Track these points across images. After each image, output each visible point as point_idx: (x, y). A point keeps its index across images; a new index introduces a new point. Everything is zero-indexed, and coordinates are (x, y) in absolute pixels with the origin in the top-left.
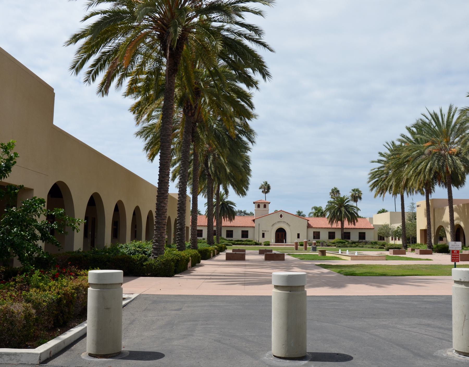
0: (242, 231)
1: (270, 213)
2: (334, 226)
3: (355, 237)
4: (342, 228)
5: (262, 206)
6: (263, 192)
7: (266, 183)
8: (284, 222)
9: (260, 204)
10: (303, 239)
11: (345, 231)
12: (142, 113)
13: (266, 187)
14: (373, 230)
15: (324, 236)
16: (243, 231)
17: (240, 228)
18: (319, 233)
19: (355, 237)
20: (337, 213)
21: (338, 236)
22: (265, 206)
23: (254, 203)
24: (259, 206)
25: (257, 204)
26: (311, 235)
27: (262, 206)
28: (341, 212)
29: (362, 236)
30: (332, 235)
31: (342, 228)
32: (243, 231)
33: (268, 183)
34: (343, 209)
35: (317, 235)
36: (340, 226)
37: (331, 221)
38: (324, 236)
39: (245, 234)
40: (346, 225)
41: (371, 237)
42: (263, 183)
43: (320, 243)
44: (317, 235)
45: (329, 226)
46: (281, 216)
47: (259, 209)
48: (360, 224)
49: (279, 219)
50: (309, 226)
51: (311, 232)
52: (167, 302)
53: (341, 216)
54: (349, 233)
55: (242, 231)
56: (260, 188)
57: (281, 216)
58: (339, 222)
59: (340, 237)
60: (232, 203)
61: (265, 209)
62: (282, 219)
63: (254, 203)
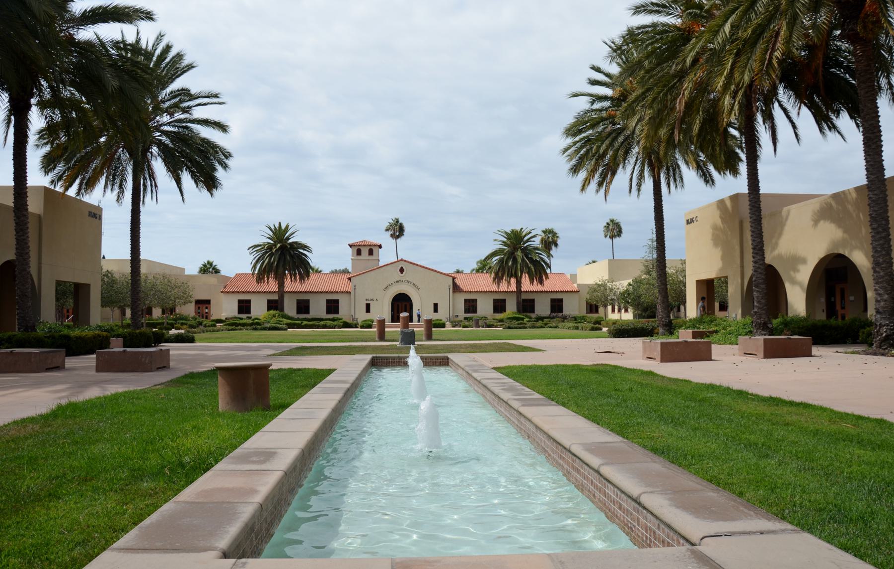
1: (381, 264)
2: (504, 287)
4: (519, 291)
5: (365, 251)
7: (397, 222)
8: (408, 282)
9: (361, 248)
11: (524, 297)
14: (576, 295)
15: (485, 308)
16: (553, 301)
17: (323, 295)
19: (543, 308)
21: (511, 308)
22: (371, 252)
24: (359, 252)
26: (461, 306)
27: (365, 251)
28: (515, 260)
30: (499, 306)
31: (519, 291)
32: (553, 301)
34: (519, 254)
35: (471, 306)
36: (513, 287)
37: (498, 279)
38: (485, 308)
39: (333, 306)
40: (527, 285)
44: (471, 306)
45: (494, 288)
46: (402, 270)
47: (359, 257)
49: (398, 276)
50: (456, 288)
51: (460, 300)
56: (387, 230)
57: (402, 270)
58: (513, 280)
59: (515, 309)
60: (305, 247)
61: (371, 257)
63: (351, 246)
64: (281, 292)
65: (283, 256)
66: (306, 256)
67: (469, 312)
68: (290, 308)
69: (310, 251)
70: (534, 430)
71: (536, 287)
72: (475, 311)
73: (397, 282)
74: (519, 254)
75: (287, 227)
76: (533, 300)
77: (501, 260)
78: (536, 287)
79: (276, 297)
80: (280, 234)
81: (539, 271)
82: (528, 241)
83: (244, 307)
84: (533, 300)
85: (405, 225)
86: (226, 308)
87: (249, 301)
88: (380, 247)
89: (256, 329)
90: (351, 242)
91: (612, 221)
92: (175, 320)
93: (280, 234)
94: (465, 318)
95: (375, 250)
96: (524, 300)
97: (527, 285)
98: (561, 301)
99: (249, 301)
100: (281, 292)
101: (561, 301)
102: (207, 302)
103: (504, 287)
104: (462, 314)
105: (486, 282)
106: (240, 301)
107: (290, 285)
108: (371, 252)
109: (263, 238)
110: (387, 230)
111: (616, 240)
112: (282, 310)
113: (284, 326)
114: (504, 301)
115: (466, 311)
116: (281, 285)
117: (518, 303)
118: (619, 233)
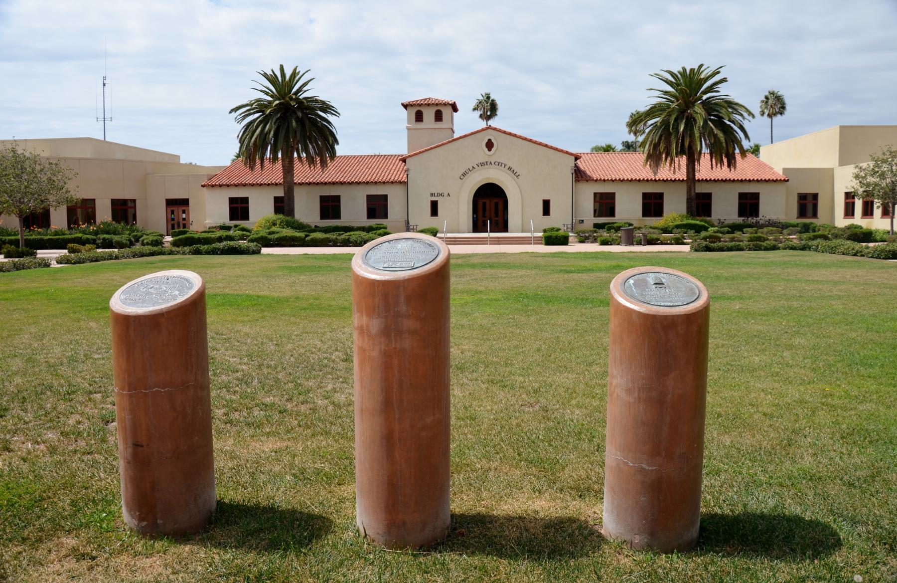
0: (369, 197)
1: (456, 136)
2: (665, 172)
3: (725, 209)
4: (691, 179)
5: (429, 115)
6: (481, 116)
7: (488, 98)
9: (423, 109)
10: (559, 219)
11: (700, 189)
12: (605, 234)
13: (488, 106)
14: (781, 187)
15: (628, 208)
16: (742, 196)
17: (361, 187)
18: (612, 196)
19: (725, 209)
20: (676, 128)
21: (675, 208)
22: (439, 117)
23: (405, 106)
24: (419, 117)
25: (414, 110)
26: (588, 205)
27: (429, 115)
28: (690, 122)
29: (749, 204)
30: (653, 205)
31: (691, 179)
32: (742, 196)
33: (492, 97)
34: (699, 110)
35: (605, 204)
36: (682, 174)
37: (654, 158)
38: (628, 208)
40: (706, 169)
41: (776, 207)
42: (481, 98)
43: (618, 229)
44: (605, 204)
45: (646, 173)
46: (490, 145)
47: (419, 125)
48: (745, 169)
49: (483, 154)
50: (579, 175)
51: (587, 193)
52: (473, 266)
53: (692, 136)
54: (709, 196)
55: (369, 197)
56: (475, 109)
57: (490, 145)
58: (684, 160)
59: (683, 208)
60: (326, 107)
61: (439, 125)
62: (495, 155)
63: (405, 106)
64: (289, 186)
65: (290, 122)
66: (329, 122)
67: (600, 216)
68: (306, 210)
69: (336, 114)
70: (551, 259)
71: (723, 172)
72: (612, 213)
73: (482, 164)
74: (699, 110)
75: (294, 74)
76: (338, 198)
77: (665, 123)
78: (723, 172)
79: (280, 193)
80: (284, 86)
81: (727, 146)
82: (710, 89)
83: (239, 209)
84: (338, 198)
85: (498, 102)
86: (209, 213)
87: (245, 200)
88: (454, 108)
89: (197, 252)
90: (405, 101)
91: (772, 93)
92: (96, 233)
93: (284, 86)
94: (597, 226)
95: (446, 112)
96: (698, 195)
97: (706, 169)
98: (756, 196)
99: (245, 200)
100: (289, 186)
101: (756, 196)
102: (185, 202)
103: (665, 172)
104: (590, 219)
105: (636, 166)
106: (232, 201)
107: (302, 172)
108: (439, 117)
109: (253, 90)
110: (475, 109)
111: (778, 119)
112: (291, 213)
113: (252, 245)
114: (660, 196)
115: (597, 213)
116: (288, 170)
117: (689, 201)
118: (783, 108)
